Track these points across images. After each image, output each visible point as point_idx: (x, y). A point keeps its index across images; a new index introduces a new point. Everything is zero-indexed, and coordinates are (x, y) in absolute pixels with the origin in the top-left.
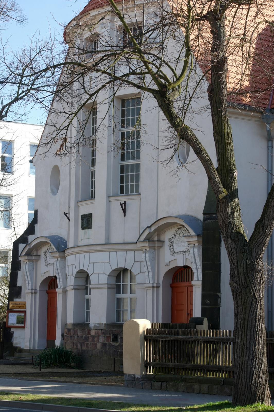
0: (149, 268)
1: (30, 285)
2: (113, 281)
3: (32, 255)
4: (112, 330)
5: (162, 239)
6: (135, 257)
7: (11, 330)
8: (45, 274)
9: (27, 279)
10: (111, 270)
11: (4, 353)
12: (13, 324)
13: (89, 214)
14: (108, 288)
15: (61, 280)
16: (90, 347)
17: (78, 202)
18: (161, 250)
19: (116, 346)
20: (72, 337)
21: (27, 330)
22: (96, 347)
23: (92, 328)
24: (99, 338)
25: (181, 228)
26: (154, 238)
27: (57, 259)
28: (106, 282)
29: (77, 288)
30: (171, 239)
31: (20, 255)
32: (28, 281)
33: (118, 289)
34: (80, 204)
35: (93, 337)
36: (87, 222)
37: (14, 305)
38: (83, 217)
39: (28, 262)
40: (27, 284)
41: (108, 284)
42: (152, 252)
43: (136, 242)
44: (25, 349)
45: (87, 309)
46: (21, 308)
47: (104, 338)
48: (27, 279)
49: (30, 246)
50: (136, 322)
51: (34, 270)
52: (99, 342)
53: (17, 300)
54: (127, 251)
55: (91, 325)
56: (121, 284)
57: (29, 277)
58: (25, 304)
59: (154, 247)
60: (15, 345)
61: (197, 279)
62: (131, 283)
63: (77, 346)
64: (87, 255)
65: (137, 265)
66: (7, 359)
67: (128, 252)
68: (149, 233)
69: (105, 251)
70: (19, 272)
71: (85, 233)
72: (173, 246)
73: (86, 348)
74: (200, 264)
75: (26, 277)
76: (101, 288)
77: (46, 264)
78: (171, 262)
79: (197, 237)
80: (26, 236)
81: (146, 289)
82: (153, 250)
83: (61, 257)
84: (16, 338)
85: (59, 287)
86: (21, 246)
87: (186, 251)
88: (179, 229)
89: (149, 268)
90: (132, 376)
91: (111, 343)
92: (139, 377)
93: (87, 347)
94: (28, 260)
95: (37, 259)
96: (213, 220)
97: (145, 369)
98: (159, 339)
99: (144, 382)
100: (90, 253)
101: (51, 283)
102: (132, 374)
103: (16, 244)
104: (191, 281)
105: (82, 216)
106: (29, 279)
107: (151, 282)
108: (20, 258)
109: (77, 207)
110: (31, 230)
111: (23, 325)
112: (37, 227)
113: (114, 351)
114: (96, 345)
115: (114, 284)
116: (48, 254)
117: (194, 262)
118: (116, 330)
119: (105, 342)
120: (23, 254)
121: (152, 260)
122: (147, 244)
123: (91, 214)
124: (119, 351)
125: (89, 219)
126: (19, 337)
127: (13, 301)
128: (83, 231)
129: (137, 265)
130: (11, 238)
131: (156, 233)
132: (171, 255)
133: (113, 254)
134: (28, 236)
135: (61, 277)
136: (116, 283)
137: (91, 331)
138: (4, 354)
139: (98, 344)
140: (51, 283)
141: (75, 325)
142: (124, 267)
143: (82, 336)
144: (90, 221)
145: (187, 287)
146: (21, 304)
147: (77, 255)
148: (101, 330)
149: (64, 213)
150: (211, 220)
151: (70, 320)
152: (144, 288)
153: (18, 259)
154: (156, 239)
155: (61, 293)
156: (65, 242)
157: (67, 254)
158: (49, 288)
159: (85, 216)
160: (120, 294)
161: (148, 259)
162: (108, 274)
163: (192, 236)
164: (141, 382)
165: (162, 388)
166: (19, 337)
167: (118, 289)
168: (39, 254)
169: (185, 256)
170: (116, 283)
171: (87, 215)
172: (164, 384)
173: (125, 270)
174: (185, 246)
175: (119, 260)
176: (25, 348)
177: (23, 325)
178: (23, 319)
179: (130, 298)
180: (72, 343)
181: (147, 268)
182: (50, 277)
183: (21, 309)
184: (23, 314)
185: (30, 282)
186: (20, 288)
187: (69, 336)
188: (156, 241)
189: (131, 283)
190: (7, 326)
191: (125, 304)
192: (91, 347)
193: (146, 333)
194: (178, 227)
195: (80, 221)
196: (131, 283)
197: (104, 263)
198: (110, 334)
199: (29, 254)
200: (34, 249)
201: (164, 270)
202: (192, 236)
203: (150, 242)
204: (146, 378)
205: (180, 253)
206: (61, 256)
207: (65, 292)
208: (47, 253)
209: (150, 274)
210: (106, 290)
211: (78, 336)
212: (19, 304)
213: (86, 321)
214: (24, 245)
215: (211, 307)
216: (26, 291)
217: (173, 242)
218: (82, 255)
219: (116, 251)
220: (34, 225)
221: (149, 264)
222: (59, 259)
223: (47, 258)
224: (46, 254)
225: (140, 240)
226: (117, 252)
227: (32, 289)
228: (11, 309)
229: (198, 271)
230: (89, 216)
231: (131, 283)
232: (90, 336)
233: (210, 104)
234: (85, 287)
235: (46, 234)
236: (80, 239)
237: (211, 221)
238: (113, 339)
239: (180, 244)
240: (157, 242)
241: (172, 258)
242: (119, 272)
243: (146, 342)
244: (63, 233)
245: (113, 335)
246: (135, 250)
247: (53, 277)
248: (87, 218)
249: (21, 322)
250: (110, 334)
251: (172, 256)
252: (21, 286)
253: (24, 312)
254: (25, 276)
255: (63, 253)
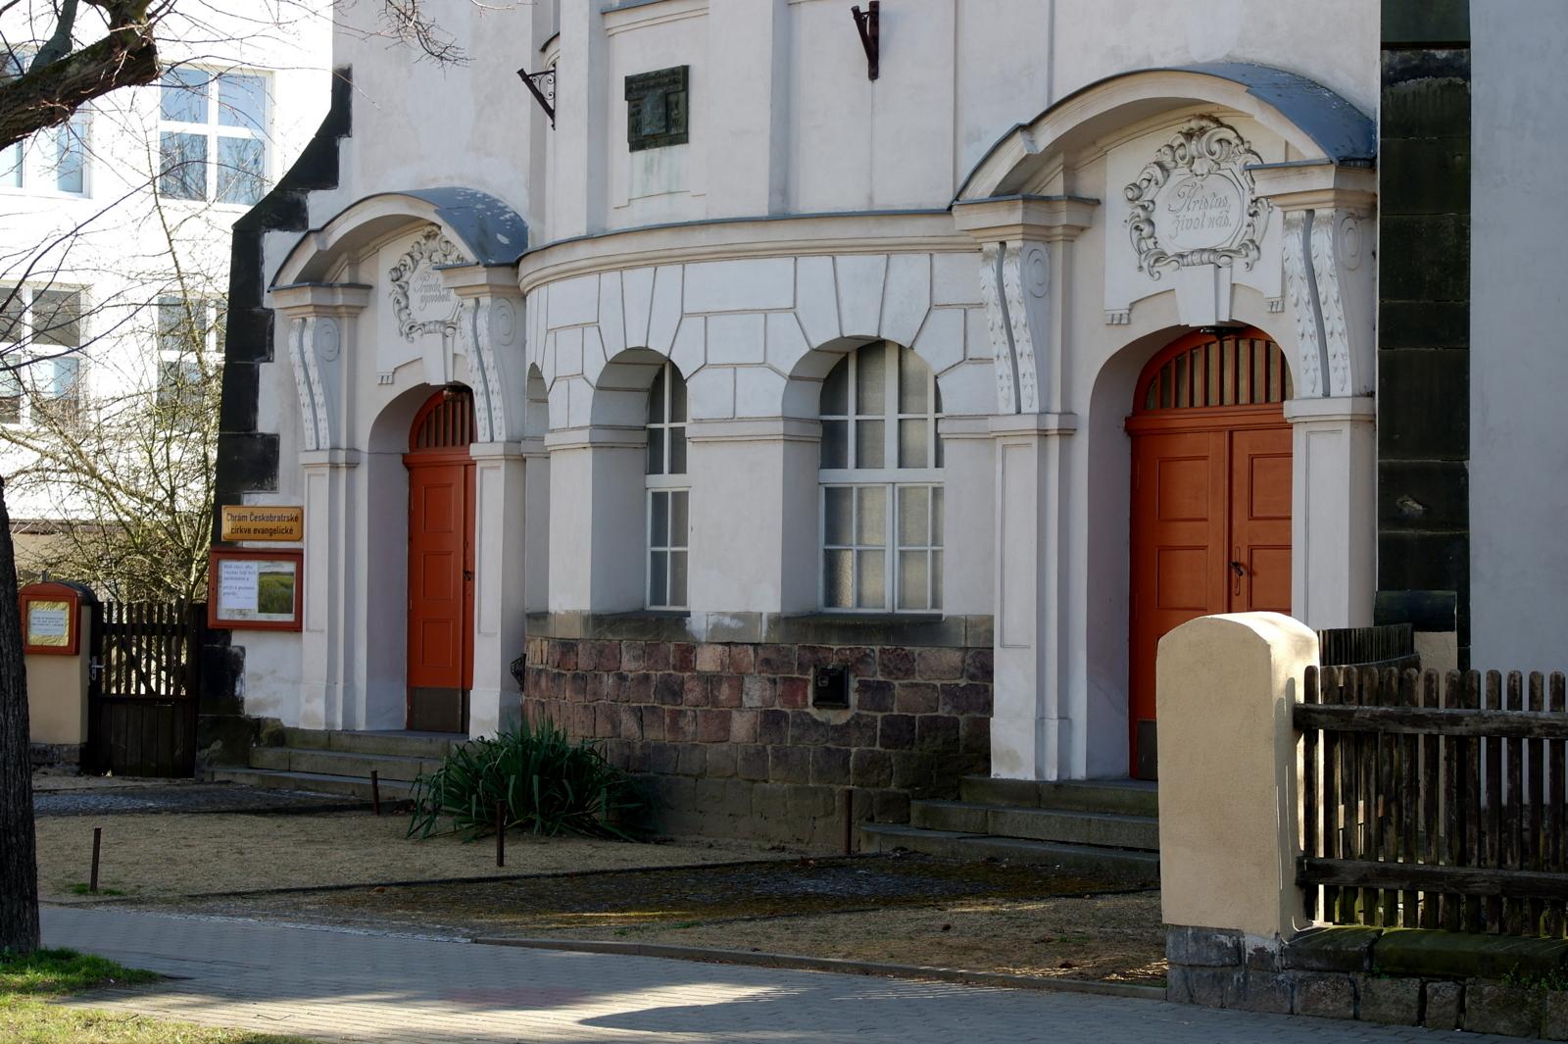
0: (1022, 336)
1: (323, 425)
2: (809, 404)
3: (331, 286)
4: (813, 649)
5: (1087, 187)
6: (935, 280)
7: (230, 639)
8: (397, 375)
9: (305, 399)
10: (806, 350)
11: (200, 749)
12: (241, 612)
13: (673, 72)
14: (788, 439)
15: (497, 401)
16: (692, 729)
17: (604, 14)
18: (1083, 246)
19: (836, 728)
20: (584, 678)
21: (314, 643)
22: (727, 730)
23: (704, 640)
24: (739, 689)
25: (1202, 131)
26: (1048, 184)
27: (477, 301)
28: (778, 412)
29: (605, 441)
30: (1139, 187)
31: (273, 285)
32: (321, 405)
33: (831, 445)
34: (615, 21)
35: (711, 680)
36: (659, 108)
37: (245, 525)
38: (636, 87)
39: (311, 320)
40: (309, 425)
41: (786, 419)
42: (1036, 255)
43: (950, 208)
44: (303, 731)
45: (655, 543)
46: (274, 536)
47: (768, 685)
48: (305, 399)
49: (324, 242)
50: (1245, 630)
51: (339, 362)
52: (740, 706)
53: (257, 500)
54: (889, 250)
55: (699, 624)
56: (851, 417)
57: (317, 389)
58: (298, 517)
59: (1049, 228)
60: (250, 710)
61: (1319, 391)
62: (902, 416)
63: (615, 724)
64: (669, 274)
65: (947, 324)
66: (218, 778)
67: (897, 260)
68: (1025, 159)
69: (771, 256)
70: (264, 368)
71: (648, 169)
72: (1151, 223)
73: (669, 737)
74: (1028, 336)
75: (303, 389)
76: (752, 440)
77: (406, 329)
78: (399, 370)
79: (1332, 169)
80: (296, 195)
81: (999, 443)
82: (1041, 246)
83: (495, 290)
84: (260, 678)
85: (482, 432)
86: (276, 244)
87: (1234, 247)
88: (1189, 135)
89: (1022, 336)
90: (1223, 938)
91: (811, 710)
92: (1272, 947)
93: (675, 728)
94: (315, 306)
95: (358, 304)
96: (1436, 77)
97: (1297, 898)
98: (1393, 728)
99: (1300, 974)
100: (600, 273)
101: (435, 419)
102: (1221, 931)
103: (246, 239)
104: (1283, 398)
105: (630, 81)
106: (319, 399)
107: (1030, 405)
108: (269, 301)
109: (601, 39)
110: (319, 164)
111: (289, 618)
112: (349, 151)
113: (828, 749)
114: (725, 720)
115: (812, 421)
116: (413, 279)
117: (301, 384)
118: (836, 648)
119: (777, 707)
120: (290, 277)
121: (1038, 294)
122: (1013, 215)
123: (685, 69)
124: (854, 750)
125: (672, 98)
126: (273, 672)
127: (237, 502)
128: (641, 155)
129: (947, 324)
130: (140, 221)
131: (1060, 159)
132: (1141, 268)
133: (816, 268)
134: (305, 192)
135: (494, 385)
136: (822, 413)
137: (699, 650)
138: (201, 754)
139: (735, 714)
140: (435, 419)
141: (597, 621)
142: (875, 335)
143: (647, 677)
144: (681, 105)
145: (1231, 433)
146: (280, 518)
147: (610, 280)
148: (751, 649)
149: (521, 72)
150: (1426, 80)
151: (571, 592)
152: (989, 438)
153: (258, 302)
154: (1056, 187)
155: (496, 464)
156: (507, 216)
157: (530, 278)
158: (415, 441)
159: (652, 83)
160: (662, 472)
161: (1013, 291)
162: (788, 371)
163: (1302, 167)
164: (1281, 977)
165: (1431, 1011)
166: (273, 672)
167: (831, 445)
168: (364, 277)
169: (1225, 272)
170: (823, 412)
171: (658, 75)
172: (1444, 992)
173: (870, 349)
174: (1227, 224)
175: (841, 299)
176: (302, 726)
177: (289, 618)
178: (288, 587)
179: (900, 490)
180: (586, 707)
181: (1005, 338)
182: (425, 387)
183: (282, 546)
184: (289, 567)
185: (322, 414)
186: (272, 442)
187: (569, 674)
188: (1058, 199)
189: (900, 412)
190: (210, 623)
191: (870, 518)
192: (695, 733)
193: (1300, 696)
194: (1185, 127)
195: (620, 109)
196: (900, 412)
197: (766, 312)
198: (802, 668)
199: (314, 277)
200: (345, 256)
201: (1098, 348)
202: (1302, 167)
203: (1032, 205)
204: (1306, 951)
205: (1196, 258)
206: (498, 286)
207: (525, 457)
208: (407, 276)
209: (1027, 366)
210: (778, 450)
211: (621, 678)
212: (271, 518)
213: (654, 602)
214: (290, 238)
215: (1428, 533)
216: (304, 458)
217: (407, 283)
218: (639, 279)
219: (833, 251)
220: (334, 141)
221: (1018, 315)
222: (486, 301)
223: (406, 296)
224: (404, 279)
225: (969, 195)
226: (839, 259)
227: (334, 448)
228: (230, 543)
229: (1021, 371)
230: (675, 82)
231: (902, 416)
232: (693, 678)
233: (48, 42)
234: (643, 437)
235: (400, 180)
236: (618, 196)
237: (1428, 86)
238: (817, 689)
239: (1195, 213)
240: (1063, 206)
241: (1146, 286)
242: (837, 358)
243: (1301, 744)
244: (501, 180)
245: (822, 673)
246: (934, 248)
247: (444, 388)
248: (660, 91)
249: (283, 605)
250: (802, 668)
251: (1145, 275)
252: (277, 435)
253: (297, 556)
254: (294, 385)
255: (508, 270)
